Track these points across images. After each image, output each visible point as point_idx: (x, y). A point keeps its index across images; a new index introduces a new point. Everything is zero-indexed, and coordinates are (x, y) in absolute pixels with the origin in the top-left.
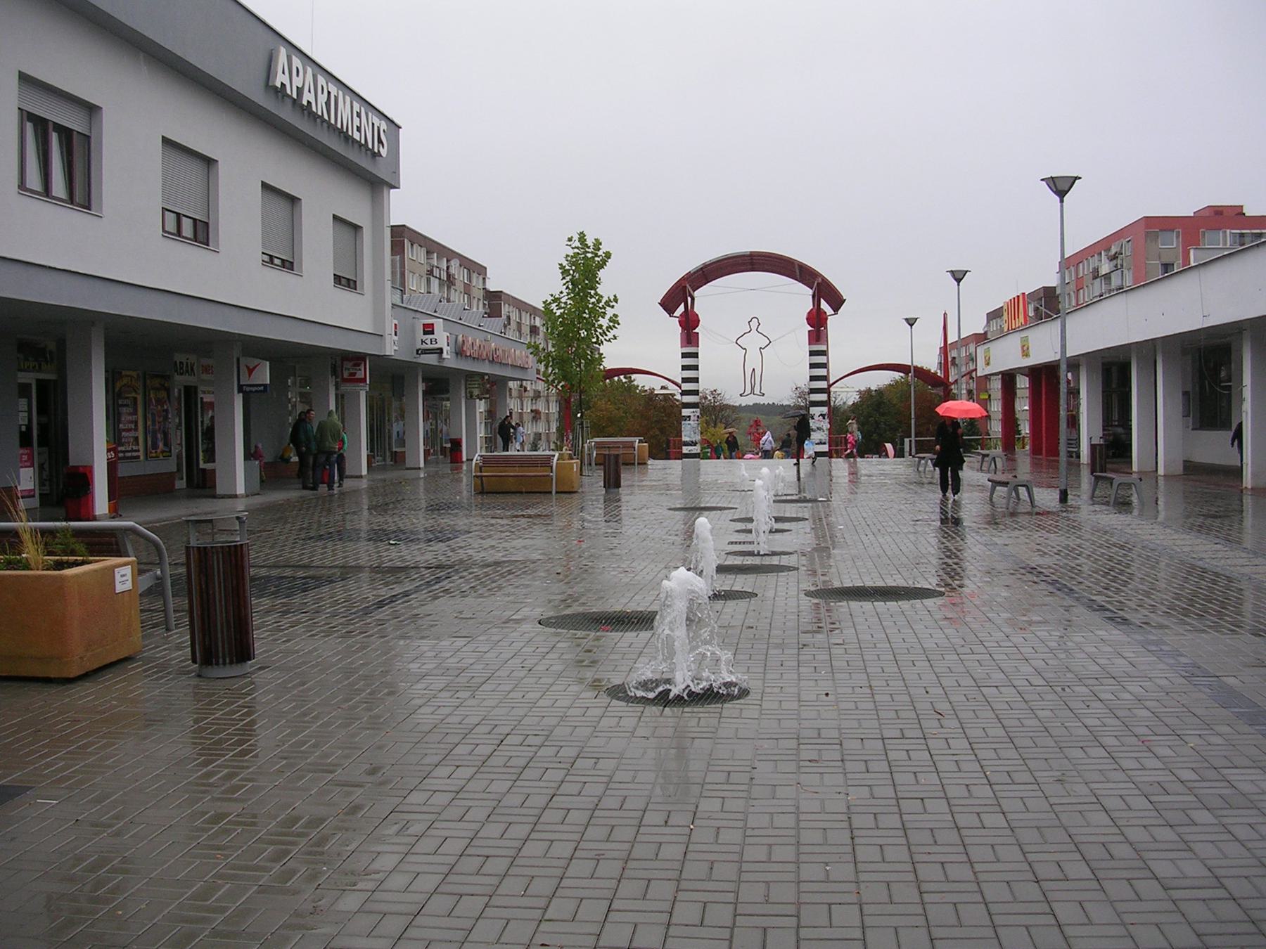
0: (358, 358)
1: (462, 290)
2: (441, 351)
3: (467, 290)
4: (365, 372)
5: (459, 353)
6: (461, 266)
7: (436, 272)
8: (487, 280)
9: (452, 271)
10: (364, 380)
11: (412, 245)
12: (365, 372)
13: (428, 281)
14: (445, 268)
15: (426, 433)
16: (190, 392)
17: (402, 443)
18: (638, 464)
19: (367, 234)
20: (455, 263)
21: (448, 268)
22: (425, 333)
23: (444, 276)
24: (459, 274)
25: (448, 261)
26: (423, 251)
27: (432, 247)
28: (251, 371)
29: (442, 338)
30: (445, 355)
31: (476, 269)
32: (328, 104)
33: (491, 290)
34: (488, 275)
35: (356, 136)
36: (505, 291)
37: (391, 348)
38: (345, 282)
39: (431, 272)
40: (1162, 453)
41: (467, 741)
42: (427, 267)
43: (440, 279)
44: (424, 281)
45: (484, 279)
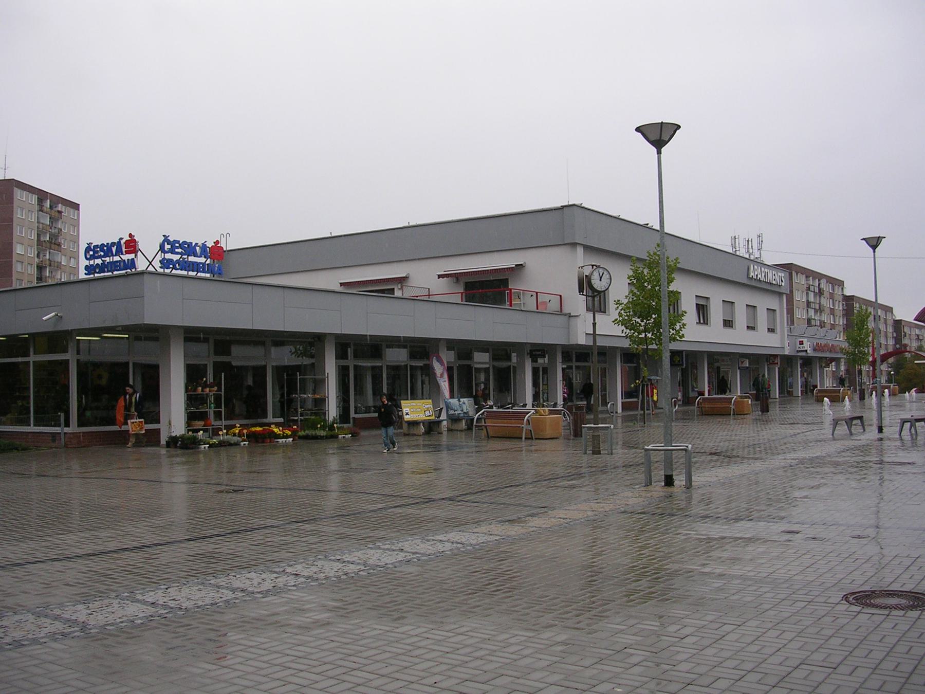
0: (775, 356)
1: (829, 297)
2: (806, 351)
3: (832, 296)
4: (778, 360)
5: (815, 350)
6: (827, 282)
7: (812, 289)
8: (844, 289)
9: (822, 286)
10: (778, 363)
11: (797, 274)
12: (778, 360)
13: (807, 294)
14: (817, 285)
15: (802, 383)
16: (718, 368)
17: (791, 387)
18: (525, 438)
19: (778, 311)
20: (823, 281)
21: (819, 285)
22: (800, 344)
23: (817, 290)
24: (826, 287)
25: (819, 280)
26: (804, 276)
27: (809, 273)
28: (742, 363)
29: (807, 346)
30: (808, 352)
31: (837, 283)
32: (765, 276)
33: (847, 295)
34: (845, 286)
35: (774, 282)
36: (856, 295)
37: (787, 352)
38: (771, 330)
39: (808, 289)
40: (268, 371)
41: (839, 635)
42: (806, 286)
43: (814, 292)
44: (805, 294)
45: (842, 289)
